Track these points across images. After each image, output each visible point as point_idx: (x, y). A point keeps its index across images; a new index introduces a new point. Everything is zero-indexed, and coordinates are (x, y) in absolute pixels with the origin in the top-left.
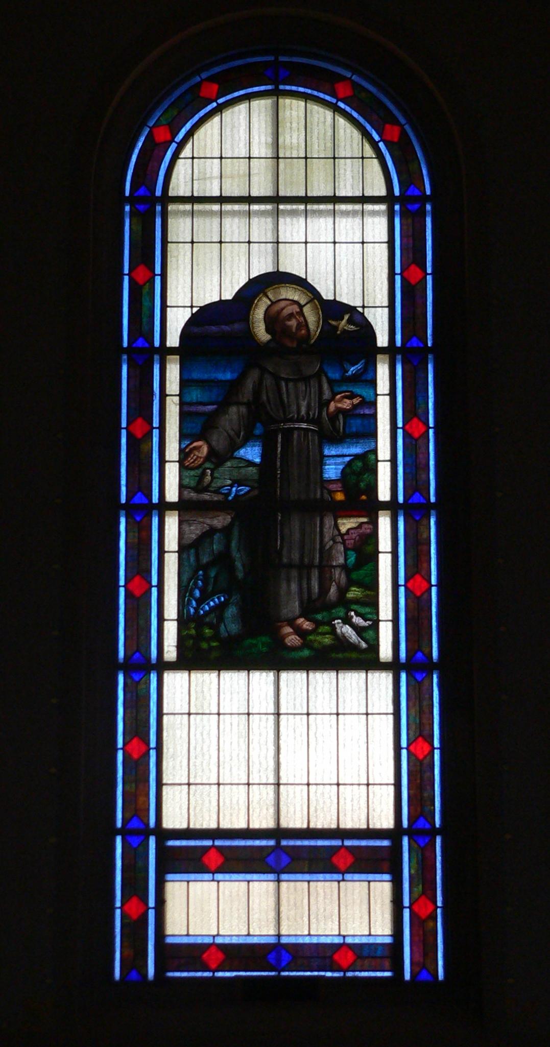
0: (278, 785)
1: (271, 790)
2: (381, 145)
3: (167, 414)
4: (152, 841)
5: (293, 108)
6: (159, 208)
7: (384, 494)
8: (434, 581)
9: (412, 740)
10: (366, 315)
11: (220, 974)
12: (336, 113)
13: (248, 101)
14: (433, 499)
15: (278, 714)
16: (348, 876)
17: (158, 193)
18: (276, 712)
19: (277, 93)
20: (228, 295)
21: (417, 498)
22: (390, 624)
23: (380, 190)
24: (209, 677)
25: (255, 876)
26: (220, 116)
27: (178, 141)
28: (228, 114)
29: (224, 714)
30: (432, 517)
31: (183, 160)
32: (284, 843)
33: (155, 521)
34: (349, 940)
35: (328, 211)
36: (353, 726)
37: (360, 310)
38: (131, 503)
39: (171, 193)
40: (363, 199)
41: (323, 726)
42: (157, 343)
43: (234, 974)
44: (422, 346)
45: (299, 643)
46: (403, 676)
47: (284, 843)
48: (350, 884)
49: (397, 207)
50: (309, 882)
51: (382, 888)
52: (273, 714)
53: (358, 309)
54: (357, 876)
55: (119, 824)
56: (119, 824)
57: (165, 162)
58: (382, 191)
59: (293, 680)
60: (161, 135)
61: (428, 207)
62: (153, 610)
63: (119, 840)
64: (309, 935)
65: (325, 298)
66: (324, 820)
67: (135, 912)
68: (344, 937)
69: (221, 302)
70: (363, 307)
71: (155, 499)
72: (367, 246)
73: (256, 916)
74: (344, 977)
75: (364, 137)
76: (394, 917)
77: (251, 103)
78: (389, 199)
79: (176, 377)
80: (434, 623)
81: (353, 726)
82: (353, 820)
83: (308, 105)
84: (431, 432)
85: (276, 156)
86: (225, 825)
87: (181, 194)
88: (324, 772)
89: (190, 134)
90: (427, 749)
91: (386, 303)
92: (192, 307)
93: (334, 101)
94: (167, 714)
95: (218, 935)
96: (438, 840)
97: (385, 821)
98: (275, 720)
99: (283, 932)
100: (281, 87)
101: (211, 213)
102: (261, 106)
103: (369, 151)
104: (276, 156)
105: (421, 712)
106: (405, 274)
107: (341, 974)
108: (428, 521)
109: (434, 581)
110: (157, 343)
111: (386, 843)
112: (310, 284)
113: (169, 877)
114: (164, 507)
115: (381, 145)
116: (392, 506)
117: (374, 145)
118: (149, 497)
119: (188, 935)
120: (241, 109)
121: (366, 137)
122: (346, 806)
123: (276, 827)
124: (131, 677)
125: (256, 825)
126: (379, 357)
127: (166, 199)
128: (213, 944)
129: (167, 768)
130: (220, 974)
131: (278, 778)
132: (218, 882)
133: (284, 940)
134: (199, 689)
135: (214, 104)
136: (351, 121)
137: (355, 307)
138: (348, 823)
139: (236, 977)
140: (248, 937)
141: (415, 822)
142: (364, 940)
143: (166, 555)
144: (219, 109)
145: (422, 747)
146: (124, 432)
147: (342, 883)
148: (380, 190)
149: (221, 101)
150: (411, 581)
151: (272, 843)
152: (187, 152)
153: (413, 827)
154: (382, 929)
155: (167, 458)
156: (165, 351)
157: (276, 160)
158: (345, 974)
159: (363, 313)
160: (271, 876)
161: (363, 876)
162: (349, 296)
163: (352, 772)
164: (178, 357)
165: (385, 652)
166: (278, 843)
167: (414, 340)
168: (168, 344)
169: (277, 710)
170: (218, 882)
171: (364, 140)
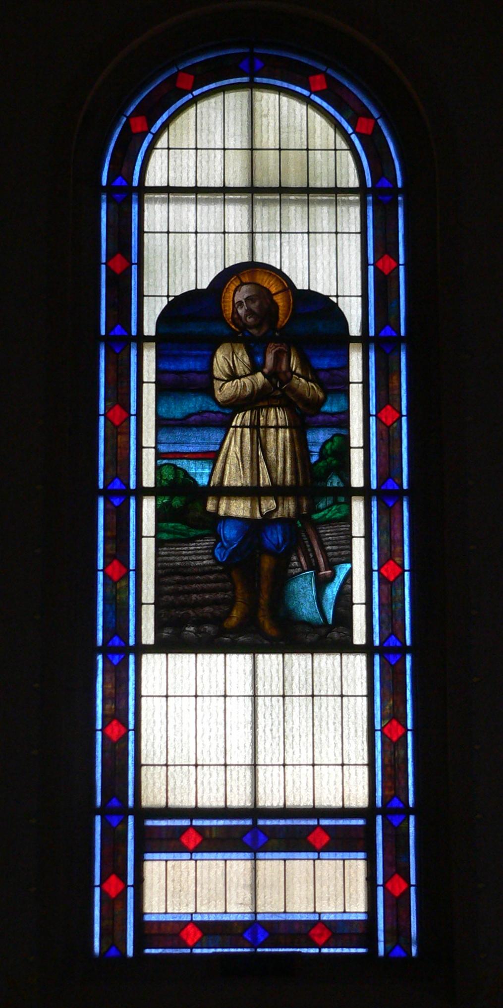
1: (249, 701)
2: (353, 137)
4: (131, 820)
5: (267, 100)
10: (340, 306)
11: (197, 951)
13: (222, 93)
14: (405, 486)
15: (255, 696)
16: (324, 855)
18: (253, 763)
19: (252, 86)
20: (204, 284)
21: (388, 332)
23: (353, 182)
24: (187, 659)
25: (234, 855)
26: (195, 107)
27: (154, 132)
28: (203, 105)
30: (399, 206)
31: (160, 150)
32: (261, 822)
35: (303, 201)
36: (328, 708)
37: (334, 299)
38: (113, 184)
39: (150, 182)
41: (298, 708)
43: (212, 951)
44: (395, 334)
45: (272, 412)
46: (377, 658)
47: (261, 822)
50: (285, 860)
51: (357, 867)
54: (332, 855)
58: (354, 182)
59: (269, 662)
60: (138, 125)
62: (133, 276)
66: (301, 799)
68: (320, 914)
69: (197, 291)
70: (337, 296)
71: (132, 485)
72: (342, 237)
74: (320, 953)
75: (337, 129)
81: (328, 708)
82: (329, 799)
84: (409, 734)
85: (253, 858)
89: (165, 126)
95: (196, 913)
96: (408, 658)
97: (359, 798)
100: (258, 80)
102: (236, 100)
104: (250, 148)
105: (391, 541)
107: (317, 950)
111: (361, 822)
113: (148, 856)
114: (141, 492)
116: (365, 492)
120: (215, 102)
121: (340, 130)
123: (250, 186)
127: (143, 190)
128: (192, 921)
130: (197, 951)
132: (196, 861)
136: (322, 113)
137: (327, 297)
140: (224, 915)
144: (195, 101)
146: (103, 267)
147: (317, 862)
148: (353, 182)
151: (249, 822)
152: (162, 142)
154: (358, 906)
156: (141, 339)
157: (250, 151)
159: (337, 304)
160: (248, 855)
162: (323, 286)
165: (359, 638)
166: (255, 822)
167: (388, 329)
168: (145, 484)
170: (196, 861)
171: (337, 135)
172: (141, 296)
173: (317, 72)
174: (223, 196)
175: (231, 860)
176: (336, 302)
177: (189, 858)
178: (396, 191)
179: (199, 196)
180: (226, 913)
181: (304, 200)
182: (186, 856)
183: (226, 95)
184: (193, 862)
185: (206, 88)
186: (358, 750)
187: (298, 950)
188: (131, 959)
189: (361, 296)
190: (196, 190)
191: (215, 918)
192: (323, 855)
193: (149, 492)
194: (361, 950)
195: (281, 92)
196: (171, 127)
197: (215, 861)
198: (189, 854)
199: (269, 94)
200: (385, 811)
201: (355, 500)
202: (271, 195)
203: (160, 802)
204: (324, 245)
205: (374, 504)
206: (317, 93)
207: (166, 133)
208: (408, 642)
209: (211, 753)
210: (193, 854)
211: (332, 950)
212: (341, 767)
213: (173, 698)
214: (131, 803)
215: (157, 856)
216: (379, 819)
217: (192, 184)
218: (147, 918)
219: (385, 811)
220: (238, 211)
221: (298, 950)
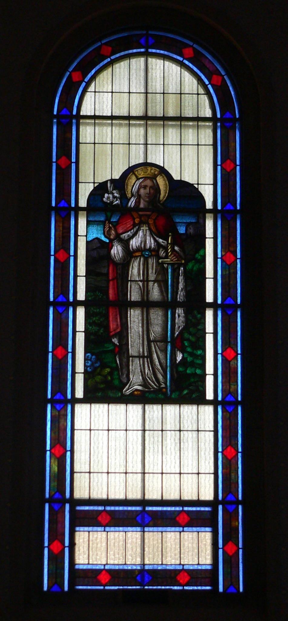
0: (144, 473)
1: (140, 476)
3: (76, 391)
4: (67, 506)
6: (74, 121)
7: (209, 298)
8: (238, 163)
9: (224, 350)
10: (199, 190)
13: (129, 58)
15: (146, 144)
19: (147, 55)
20: (117, 176)
22: (212, 335)
25: (130, 529)
28: (117, 66)
34: (186, 567)
37: (196, 186)
40: (198, 119)
42: (73, 205)
43: (117, 588)
49: (219, 124)
51: (206, 536)
52: (142, 430)
63: (47, 506)
65: (175, 179)
67: (56, 544)
68: (183, 565)
70: (198, 184)
73: (130, 541)
76: (213, 552)
77: (131, 60)
80: (239, 334)
82: (189, 495)
84: (240, 455)
86: (112, 497)
87: (89, 114)
88: (171, 466)
89: (93, 78)
90: (235, 548)
93: (181, 59)
94: (77, 430)
95: (107, 564)
97: (208, 495)
98: (142, 434)
100: (150, 50)
102: (138, 63)
103: (201, 91)
108: (235, 144)
109: (238, 163)
110: (73, 205)
112: (166, 170)
114: (76, 303)
116: (214, 305)
117: (205, 87)
122: (185, 487)
124: (55, 408)
126: (207, 215)
127: (79, 117)
128: (104, 569)
129: (77, 458)
131: (146, 140)
133: (147, 567)
135: (109, 60)
138: (187, 496)
139: (118, 589)
141: (225, 300)
143: (77, 375)
144: (112, 63)
148: (208, 113)
149: (113, 57)
151: (138, 508)
152: (92, 88)
154: (206, 560)
156: (77, 209)
159: (198, 188)
160: (139, 529)
162: (189, 178)
163: (190, 466)
164: (86, 206)
165: (210, 395)
166: (144, 508)
170: (107, 532)
173: (187, 46)
176: (197, 187)
177: (103, 530)
179: (96, 121)
192: (185, 529)
193: (81, 303)
196: (97, 80)
198: (103, 528)
204: (190, 152)
207: (94, 82)
208: (239, 399)
209: (117, 465)
214: (68, 495)
216: (220, 507)
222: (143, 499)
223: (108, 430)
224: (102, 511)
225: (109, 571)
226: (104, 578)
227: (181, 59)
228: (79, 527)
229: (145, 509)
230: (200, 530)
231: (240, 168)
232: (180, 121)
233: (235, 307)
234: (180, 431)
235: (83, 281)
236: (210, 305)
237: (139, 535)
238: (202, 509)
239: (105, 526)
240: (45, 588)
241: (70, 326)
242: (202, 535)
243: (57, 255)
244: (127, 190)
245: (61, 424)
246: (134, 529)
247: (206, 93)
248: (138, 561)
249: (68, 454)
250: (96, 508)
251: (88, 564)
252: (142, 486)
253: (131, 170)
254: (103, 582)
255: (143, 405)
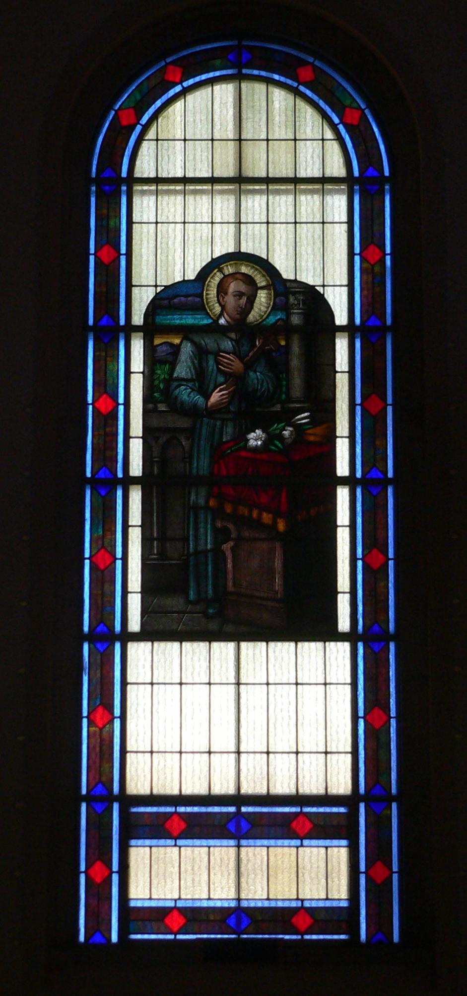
1: (232, 688)
2: (341, 127)
4: (116, 806)
6: (124, 188)
12: (297, 96)
17: (124, 174)
19: (239, 78)
20: (191, 275)
22: (347, 596)
28: (190, 98)
29: (186, 752)
32: (244, 809)
33: (119, 493)
34: (307, 904)
36: (311, 696)
37: (320, 289)
39: (138, 174)
42: (122, 322)
46: (359, 491)
47: (244, 809)
48: (308, 850)
49: (356, 187)
51: (340, 853)
52: (235, 752)
53: (317, 288)
54: (314, 842)
55: (84, 791)
56: (84, 791)
57: (129, 148)
61: (387, 187)
64: (268, 899)
65: (285, 276)
66: (283, 787)
67: (98, 866)
70: (324, 286)
75: (324, 120)
78: (348, 180)
79: (139, 465)
81: (311, 696)
82: (312, 786)
83: (269, 87)
86: (188, 790)
91: (345, 282)
92: (156, 286)
93: (295, 84)
95: (180, 899)
96: (390, 491)
97: (342, 785)
99: (243, 896)
100: (244, 71)
101: (176, 192)
102: (225, 92)
103: (329, 134)
106: (364, 254)
107: (299, 937)
110: (122, 322)
113: (133, 842)
114: (128, 481)
115: (341, 127)
117: (334, 127)
118: (115, 398)
119: (150, 899)
121: (326, 120)
125: (217, 790)
127: (132, 180)
128: (175, 908)
132: (180, 847)
133: (244, 904)
134: (164, 258)
137: (313, 287)
139: (197, 939)
142: (321, 904)
145: (375, 256)
148: (337, 168)
150: (366, 252)
151: (232, 809)
152: (151, 134)
153: (367, 477)
154: (340, 892)
155: (128, 749)
156: (130, 329)
158: (302, 937)
160: (232, 842)
161: (321, 842)
162: (309, 278)
163: (311, 740)
164: (141, 475)
165: (344, 624)
166: (239, 809)
167: (371, 169)
169: (237, 895)
170: (180, 847)
172: (129, 286)
173: (305, 63)
174: (183, 187)
175: (215, 846)
177: (173, 844)
178: (383, 180)
179: (159, 188)
180: (327, 899)
181: (207, 190)
182: (171, 842)
183: (215, 87)
184: (178, 848)
185: (198, 79)
186: (342, 739)
187: (281, 936)
188: (396, 944)
189: (351, 753)
190: (184, 180)
191: (310, 904)
194: (343, 937)
195: (269, 82)
197: (309, 848)
199: (260, 85)
200: (367, 798)
201: (339, 488)
202: (281, 185)
203: (144, 790)
205: (359, 491)
206: (305, 85)
209: (196, 740)
210: (178, 841)
211: (314, 937)
212: (295, 755)
213: (163, 686)
215: (140, 842)
217: (264, 175)
218: (133, 904)
219: (367, 798)
220: (226, 203)
221: (281, 936)
222: (237, 175)
223: (181, 684)
224: (172, 814)
225: (183, 911)
226: (177, 921)
227: (295, 84)
228: (136, 840)
229: (240, 810)
230: (330, 845)
231: (399, 877)
232: (293, 184)
233: (383, 330)
234: (297, 753)
235: (138, 504)
236: (343, 481)
237: (232, 851)
238: (335, 810)
239: (176, 839)
240: (82, 938)
241: (117, 612)
242: (334, 851)
243: (97, 405)
244: (207, 304)
245: (112, 223)
246: (225, 842)
247: (336, 138)
248: (232, 894)
249: (121, 408)
250: (162, 809)
251: (150, 899)
252: (235, 698)
253: (215, 264)
254: (176, 818)
255: (236, 642)
